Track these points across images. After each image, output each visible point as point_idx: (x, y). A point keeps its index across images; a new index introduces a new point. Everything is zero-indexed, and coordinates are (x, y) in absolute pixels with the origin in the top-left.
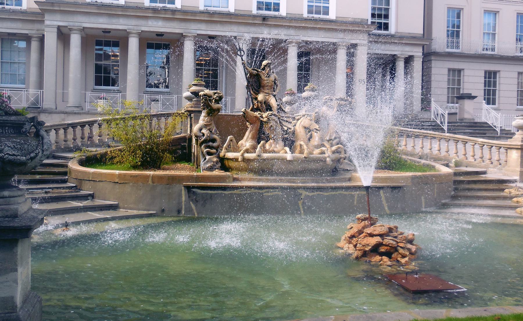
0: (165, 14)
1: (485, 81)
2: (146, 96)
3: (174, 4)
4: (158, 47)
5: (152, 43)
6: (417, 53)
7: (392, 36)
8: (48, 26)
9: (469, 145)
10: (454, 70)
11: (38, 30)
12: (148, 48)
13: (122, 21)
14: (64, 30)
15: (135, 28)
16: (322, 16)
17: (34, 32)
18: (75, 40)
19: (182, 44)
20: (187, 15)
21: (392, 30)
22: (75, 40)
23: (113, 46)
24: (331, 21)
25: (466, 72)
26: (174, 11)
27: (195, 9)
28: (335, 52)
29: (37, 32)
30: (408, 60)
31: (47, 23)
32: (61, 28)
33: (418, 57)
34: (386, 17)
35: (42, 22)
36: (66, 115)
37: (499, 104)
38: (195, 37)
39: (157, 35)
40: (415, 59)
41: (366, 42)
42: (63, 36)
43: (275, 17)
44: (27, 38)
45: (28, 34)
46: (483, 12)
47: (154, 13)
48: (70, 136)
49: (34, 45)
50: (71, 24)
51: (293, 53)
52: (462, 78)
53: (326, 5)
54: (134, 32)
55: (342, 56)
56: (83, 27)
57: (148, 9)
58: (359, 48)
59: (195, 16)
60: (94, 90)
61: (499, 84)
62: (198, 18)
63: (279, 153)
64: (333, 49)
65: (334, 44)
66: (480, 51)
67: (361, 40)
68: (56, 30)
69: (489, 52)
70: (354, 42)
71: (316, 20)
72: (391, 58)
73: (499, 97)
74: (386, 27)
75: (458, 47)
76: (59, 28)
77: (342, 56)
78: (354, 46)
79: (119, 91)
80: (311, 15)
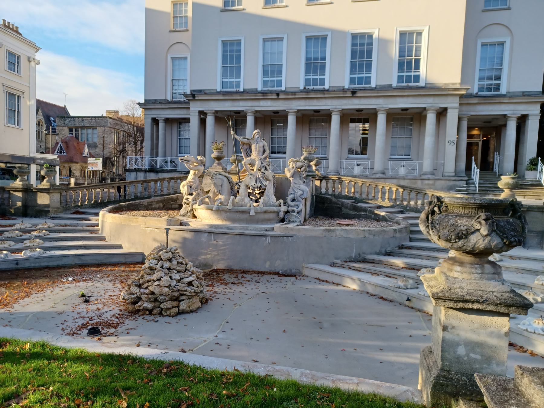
0: (272, 95)
2: (391, 163)
4: (359, 121)
5: (349, 117)
7: (504, 96)
8: (193, 111)
9: (330, 192)
12: (351, 122)
13: (241, 103)
16: (412, 84)
18: (210, 120)
20: (288, 95)
21: (503, 90)
22: (210, 120)
23: (358, 122)
24: (372, 89)
26: (324, 91)
31: (191, 109)
34: (498, 78)
35: (189, 108)
40: (530, 118)
43: (365, 89)
47: (264, 96)
50: (207, 109)
54: (249, 111)
55: (431, 118)
57: (219, 93)
59: (295, 95)
60: (348, 159)
62: (200, 98)
71: (314, 91)
74: (498, 88)
77: (431, 118)
78: (445, 110)
79: (367, 159)
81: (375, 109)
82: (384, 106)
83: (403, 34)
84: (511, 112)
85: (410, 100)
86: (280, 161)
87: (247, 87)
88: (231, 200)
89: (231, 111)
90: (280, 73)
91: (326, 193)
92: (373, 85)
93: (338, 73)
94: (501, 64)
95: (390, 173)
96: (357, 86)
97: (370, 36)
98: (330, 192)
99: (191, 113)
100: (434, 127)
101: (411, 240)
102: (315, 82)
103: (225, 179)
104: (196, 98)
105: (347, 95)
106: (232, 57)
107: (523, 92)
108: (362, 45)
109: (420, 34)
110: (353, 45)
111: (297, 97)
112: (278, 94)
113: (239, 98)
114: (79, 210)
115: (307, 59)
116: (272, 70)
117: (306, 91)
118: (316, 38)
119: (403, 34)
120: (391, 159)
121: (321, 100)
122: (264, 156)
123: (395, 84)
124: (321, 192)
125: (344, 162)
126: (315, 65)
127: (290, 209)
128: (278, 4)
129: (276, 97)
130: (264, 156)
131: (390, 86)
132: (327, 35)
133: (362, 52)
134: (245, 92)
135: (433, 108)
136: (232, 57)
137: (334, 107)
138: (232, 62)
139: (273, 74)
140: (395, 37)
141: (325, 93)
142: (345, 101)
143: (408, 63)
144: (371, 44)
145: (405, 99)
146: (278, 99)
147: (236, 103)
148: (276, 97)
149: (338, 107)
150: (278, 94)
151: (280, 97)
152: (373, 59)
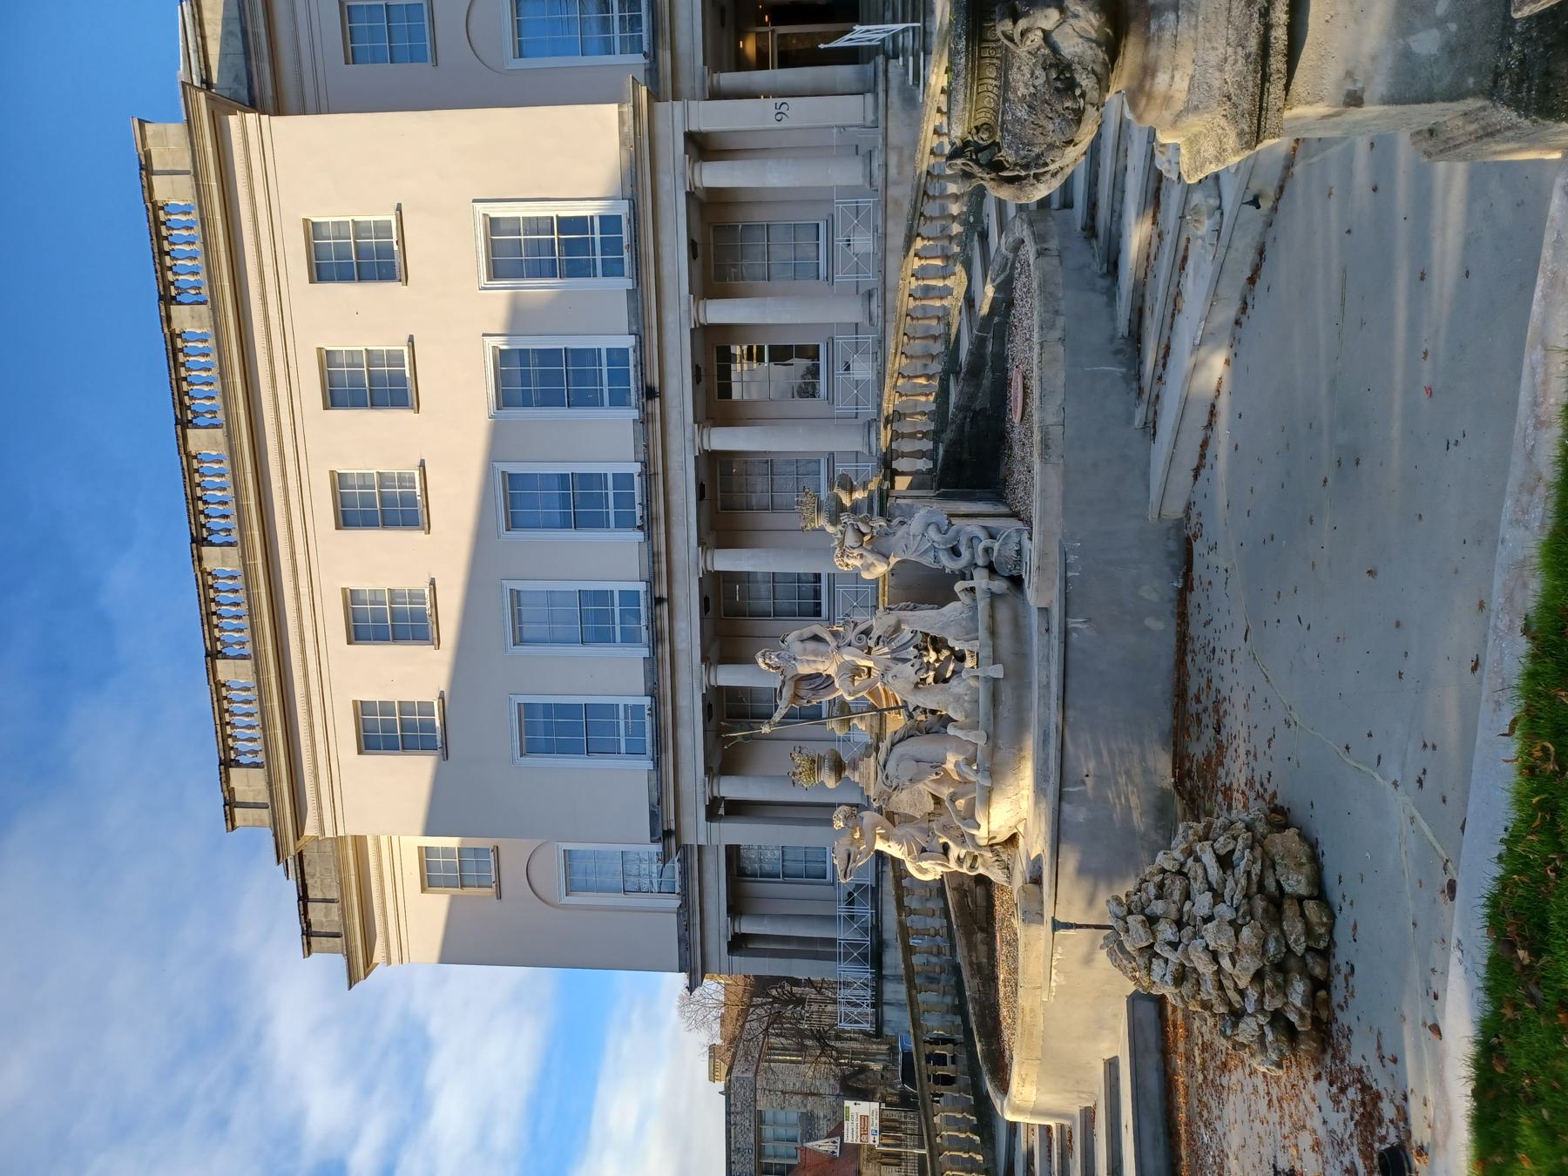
2: (839, 277)
5: (717, 403)
13: (683, 701)
18: (731, 788)
19: (710, 190)
38: (708, 669)
47: (662, 641)
54: (705, 679)
55: (715, 176)
59: (659, 554)
63: (977, 690)
77: (715, 176)
85: (666, 238)
86: (840, 589)
87: (640, 684)
88: (959, 733)
89: (705, 731)
92: (629, 342)
96: (631, 367)
98: (927, 445)
103: (899, 749)
109: (494, 224)
110: (527, 403)
112: (659, 601)
116: (594, 618)
118: (511, 502)
120: (830, 278)
122: (828, 637)
123: (626, 283)
124: (930, 471)
125: (841, 408)
126: (577, 502)
127: (980, 562)
129: (666, 606)
130: (828, 637)
131: (631, 294)
134: (653, 692)
137: (689, 444)
142: (682, 661)
145: (666, 252)
146: (670, 600)
148: (666, 606)
149: (689, 434)
150: (659, 601)
151: (665, 596)
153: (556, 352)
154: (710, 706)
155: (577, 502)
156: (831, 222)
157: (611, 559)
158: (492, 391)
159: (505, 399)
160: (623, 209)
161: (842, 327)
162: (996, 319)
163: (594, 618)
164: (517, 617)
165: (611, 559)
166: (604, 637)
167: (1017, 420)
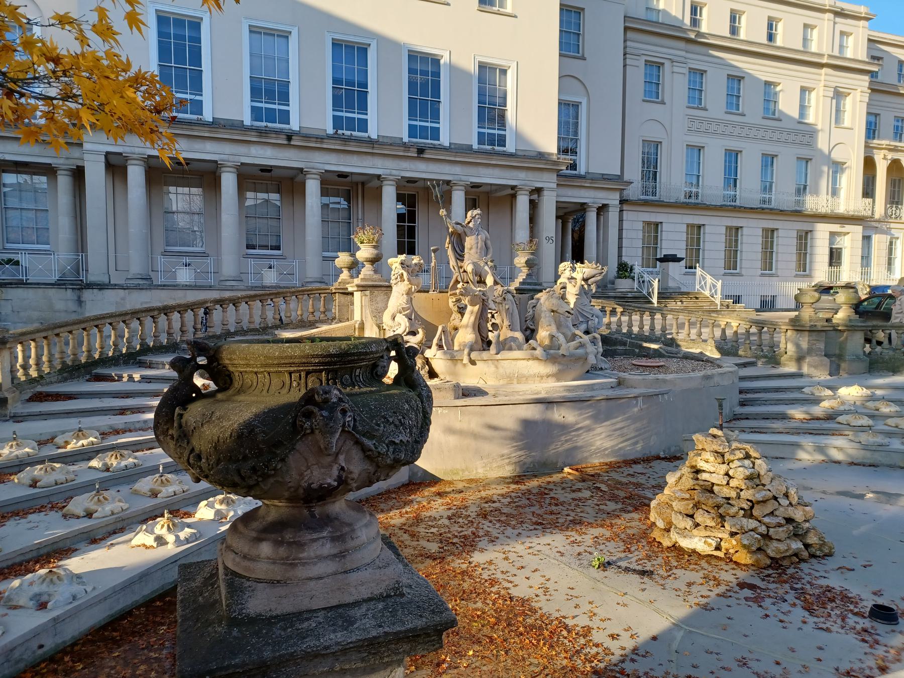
0: (277, 138)
1: (687, 238)
2: (251, 262)
3: (439, 140)
5: (252, 178)
6: (613, 199)
9: (625, 331)
10: (649, 223)
11: (67, 158)
13: (210, 146)
14: (114, 160)
15: (231, 158)
17: (61, 161)
18: (136, 174)
19: (303, 184)
22: (136, 174)
25: (745, 231)
27: (322, 134)
28: (514, 196)
29: (67, 162)
30: (602, 209)
31: (86, 146)
32: (110, 156)
33: (614, 206)
36: (127, 291)
37: (776, 269)
38: (466, 186)
39: (262, 170)
40: (611, 209)
41: (555, 186)
42: (116, 167)
44: (49, 171)
45: (50, 164)
46: (685, 147)
48: (176, 325)
49: (64, 182)
50: (127, 149)
51: (389, 193)
52: (775, 239)
53: (198, 98)
54: (230, 164)
55: (523, 202)
56: (242, 164)
57: (250, 129)
58: (545, 193)
59: (322, 142)
61: (704, 242)
64: (512, 194)
65: (513, 187)
66: (682, 199)
67: (548, 181)
68: (103, 158)
69: (693, 200)
70: (539, 185)
72: (579, 207)
73: (777, 261)
75: (654, 194)
76: (107, 154)
77: (523, 202)
78: (538, 191)
80: (414, 140)
81: (216, 162)
82: (464, 178)
83: (482, 67)
84: (591, 200)
85: (497, 172)
87: (222, 115)
89: (491, 185)
90: (285, 97)
91: (630, 332)
92: (207, 116)
93: (387, 113)
94: (576, 133)
95: (159, 280)
96: (429, 141)
97: (436, 61)
98: (636, 329)
99: (86, 156)
100: (144, 190)
101: (743, 404)
102: (271, 116)
104: (292, 143)
105: (409, 154)
106: (180, 50)
107: (603, 175)
108: (424, 73)
109: (504, 72)
110: (411, 71)
111: (325, 146)
112: (289, 138)
113: (207, 135)
114: (39, 389)
115: (336, 81)
116: (269, 90)
117: (334, 137)
118: (350, 46)
119: (482, 67)
120: (247, 256)
121: (364, 157)
123: (248, 121)
125: (161, 261)
126: (350, 94)
128: (495, 9)
129: (285, 142)
131: (470, 147)
132: (369, 45)
133: (424, 85)
134: (216, 124)
135: (527, 188)
136: (180, 50)
138: (180, 59)
139: (271, 96)
140: (473, 69)
141: (374, 147)
142: (405, 164)
143: (492, 111)
144: (437, 74)
145: (489, 171)
146: (289, 146)
147: (198, 145)
148: (285, 142)
149: (394, 172)
150: (289, 138)
151: (292, 143)
152: (442, 99)
153: (437, 92)
154: (270, 171)
155: (350, 94)
156: (282, 258)
157: (311, 107)
158: (419, 49)
159: (414, 57)
160: (510, 147)
161: (218, 263)
162: (637, 350)
163: (269, 90)
164: (270, 33)
165: (311, 107)
166: (255, 93)
167: (634, 362)
